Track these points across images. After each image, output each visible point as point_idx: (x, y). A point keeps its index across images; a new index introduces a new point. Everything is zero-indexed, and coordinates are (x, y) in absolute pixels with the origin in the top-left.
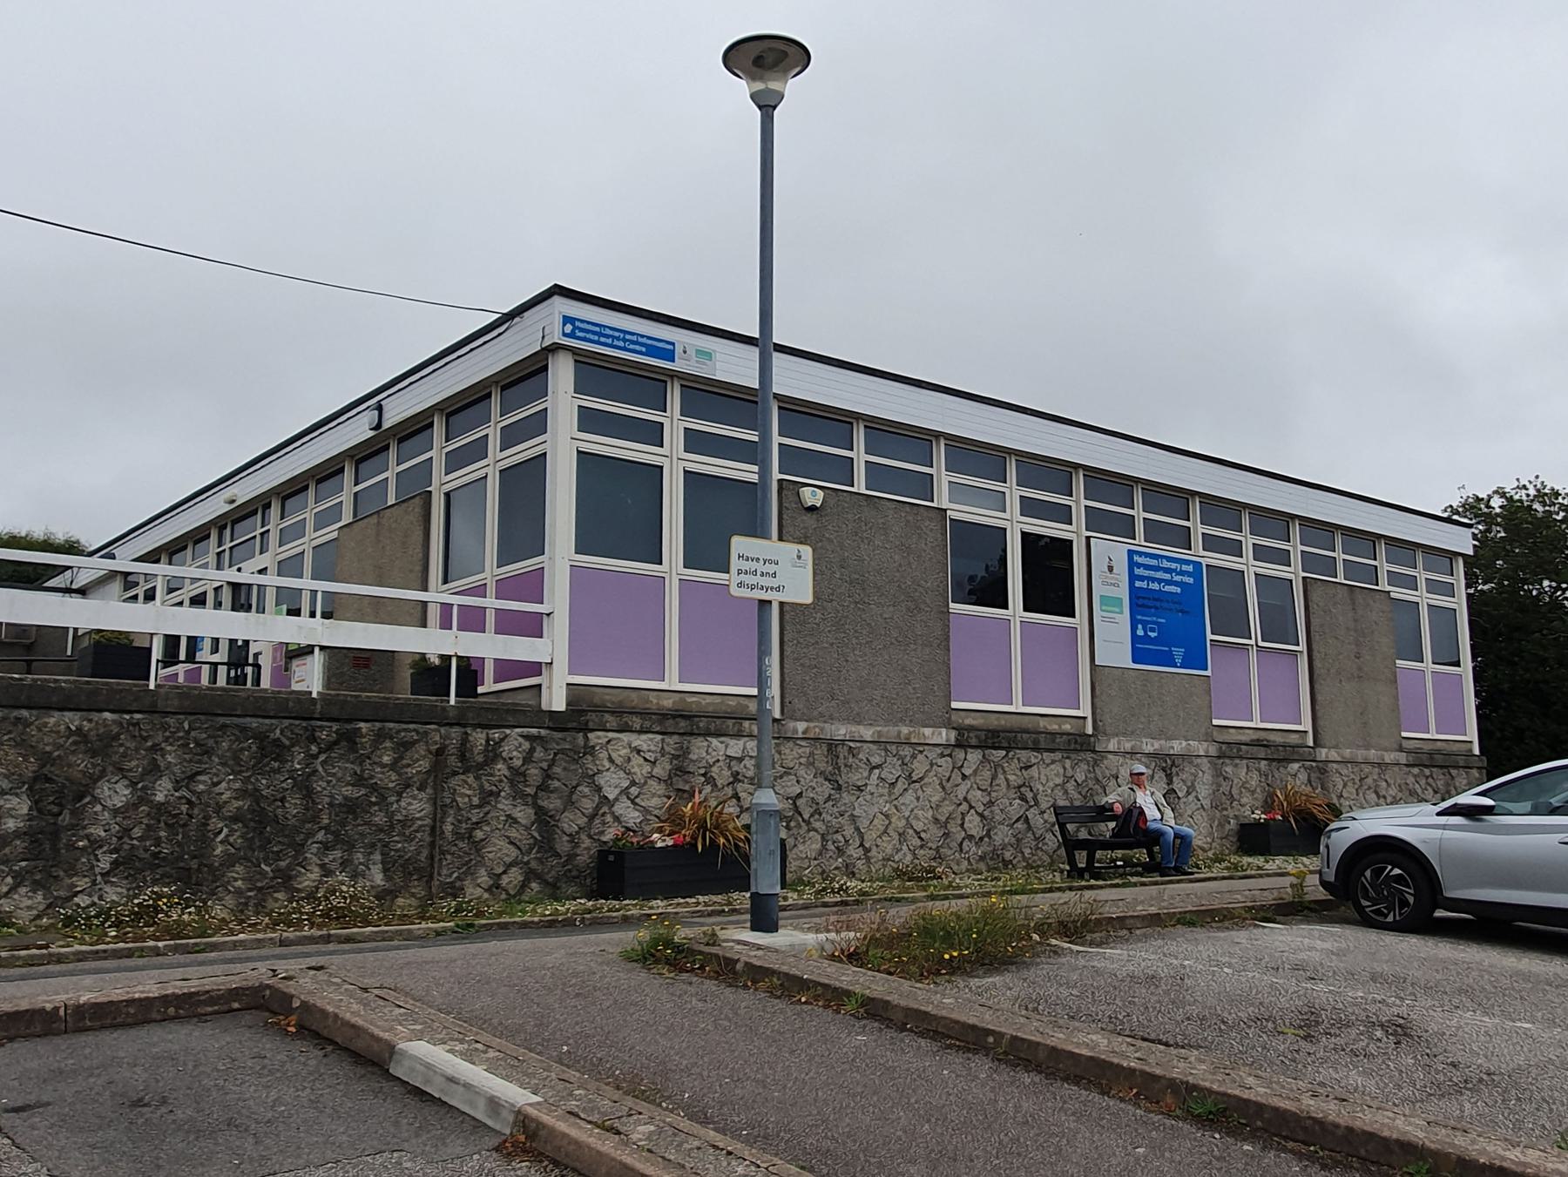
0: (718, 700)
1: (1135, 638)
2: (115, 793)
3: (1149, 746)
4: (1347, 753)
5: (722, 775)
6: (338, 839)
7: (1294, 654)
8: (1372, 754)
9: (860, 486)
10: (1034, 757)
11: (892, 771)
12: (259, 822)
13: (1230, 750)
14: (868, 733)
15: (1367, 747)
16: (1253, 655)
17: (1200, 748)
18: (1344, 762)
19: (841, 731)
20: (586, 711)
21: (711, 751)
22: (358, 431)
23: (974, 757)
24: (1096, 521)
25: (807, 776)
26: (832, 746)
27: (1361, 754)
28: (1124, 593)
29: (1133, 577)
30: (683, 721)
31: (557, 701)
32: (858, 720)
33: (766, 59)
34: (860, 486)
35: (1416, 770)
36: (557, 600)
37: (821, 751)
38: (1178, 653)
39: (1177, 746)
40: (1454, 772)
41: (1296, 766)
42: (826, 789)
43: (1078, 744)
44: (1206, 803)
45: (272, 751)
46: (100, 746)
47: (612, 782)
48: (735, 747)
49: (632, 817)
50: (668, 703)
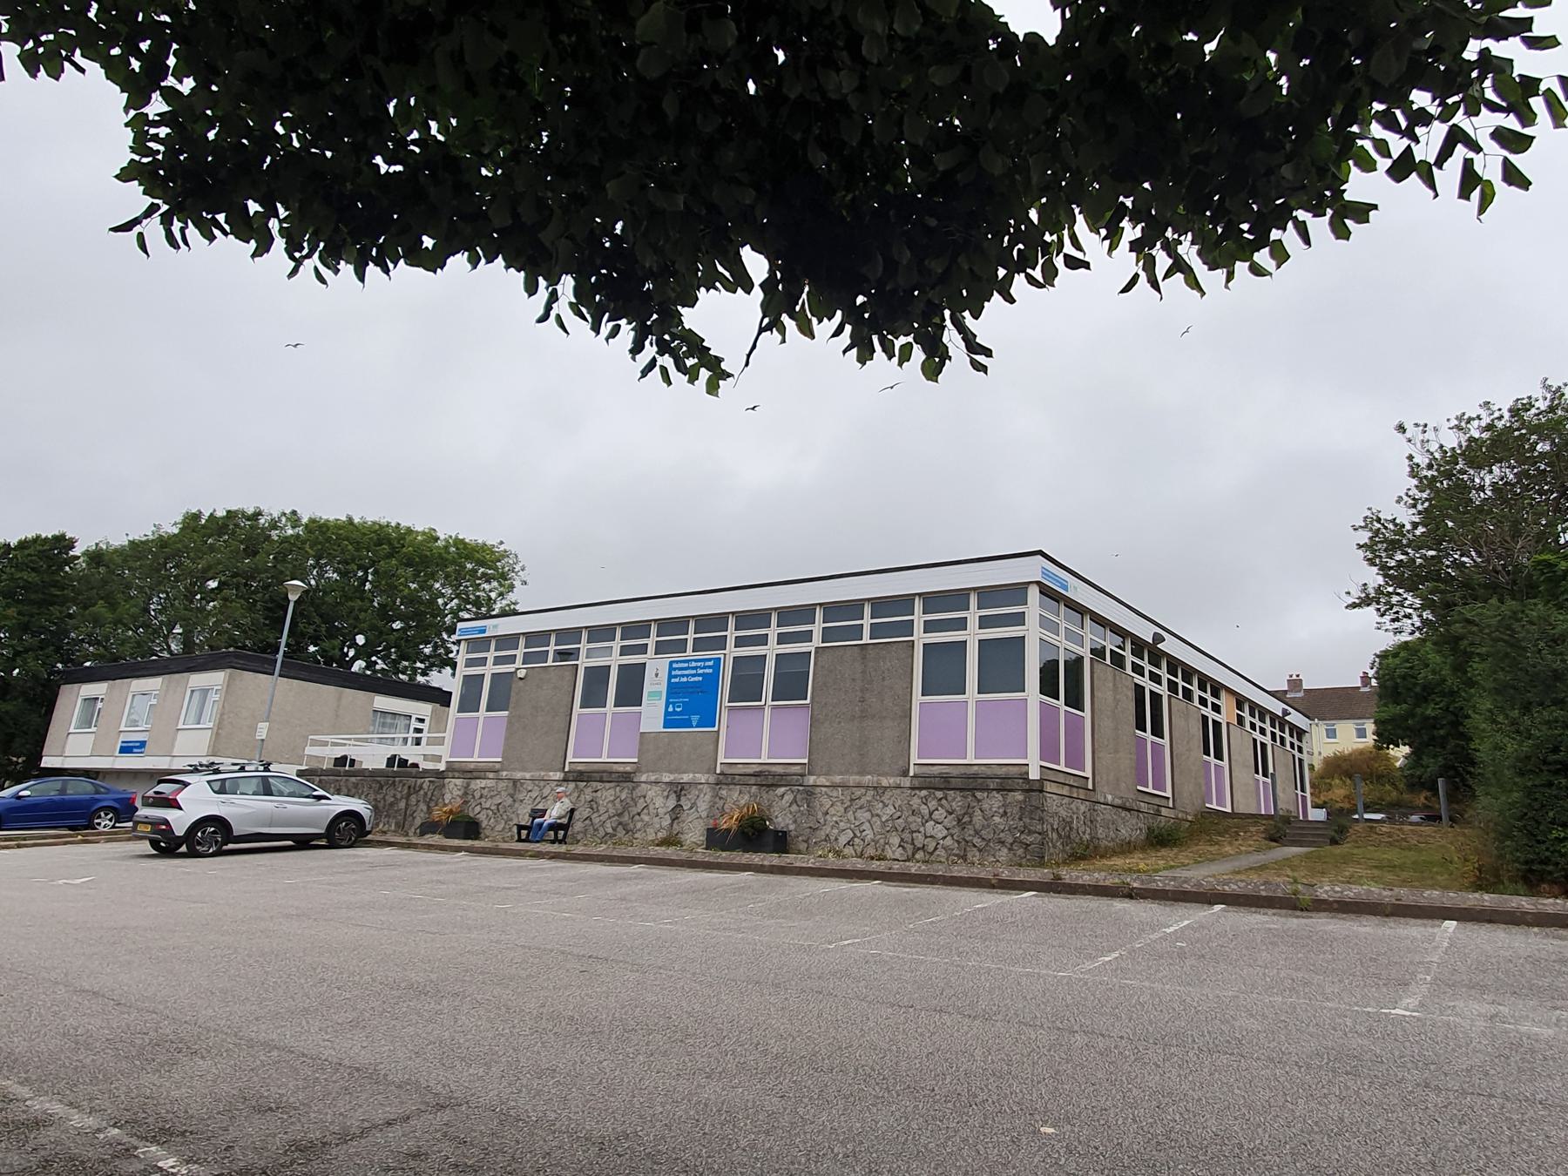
0: (1016, 769)
1: (667, 713)
3: (667, 778)
4: (838, 779)
5: (477, 795)
6: (388, 816)
7: (762, 708)
8: (867, 779)
10: (599, 785)
13: (727, 779)
14: (528, 776)
15: (862, 773)
16: (767, 711)
17: (702, 778)
18: (834, 786)
19: (518, 775)
21: (477, 784)
22: (1146, 633)
26: (515, 782)
27: (853, 779)
28: (664, 688)
30: (470, 773)
32: (524, 769)
35: (924, 793)
36: (448, 735)
38: (695, 719)
39: (686, 778)
40: (978, 794)
41: (783, 789)
42: (510, 801)
43: (625, 778)
44: (704, 814)
50: (472, 766)
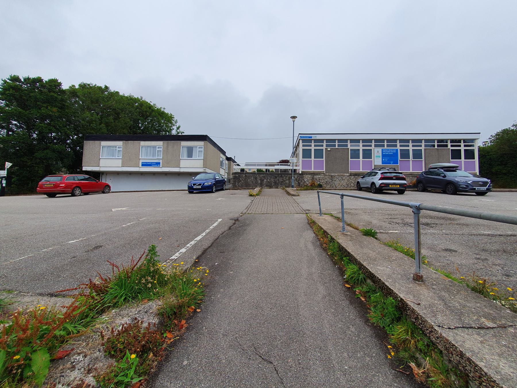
2: (265, 180)
5: (318, 179)
6: (281, 184)
9: (337, 147)
11: (340, 178)
12: (275, 183)
19: (333, 174)
20: (303, 173)
23: (353, 177)
24: (376, 146)
25: (328, 179)
26: (332, 176)
29: (382, 153)
30: (314, 174)
31: (300, 173)
33: (294, 117)
34: (436, 147)
37: (330, 177)
45: (276, 177)
46: (264, 177)
47: (306, 180)
48: (319, 176)
49: (308, 183)
